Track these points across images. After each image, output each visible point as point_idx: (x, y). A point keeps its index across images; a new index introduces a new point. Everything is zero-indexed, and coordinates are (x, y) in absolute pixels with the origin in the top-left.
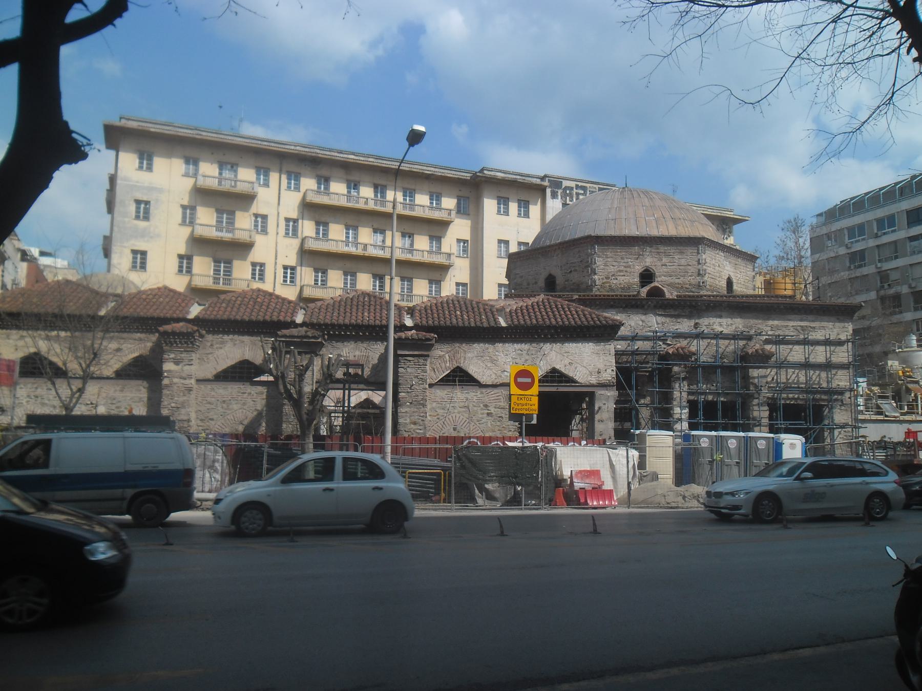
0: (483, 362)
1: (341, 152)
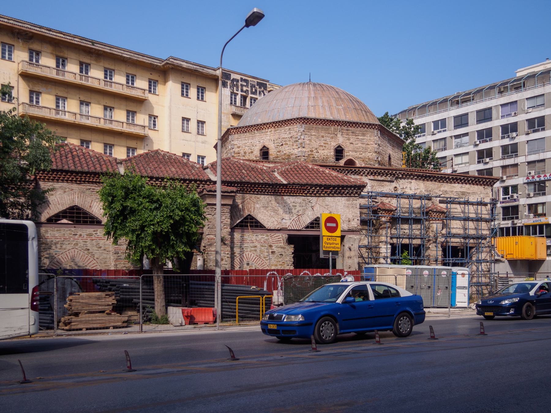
0: (267, 211)
1: (50, 30)
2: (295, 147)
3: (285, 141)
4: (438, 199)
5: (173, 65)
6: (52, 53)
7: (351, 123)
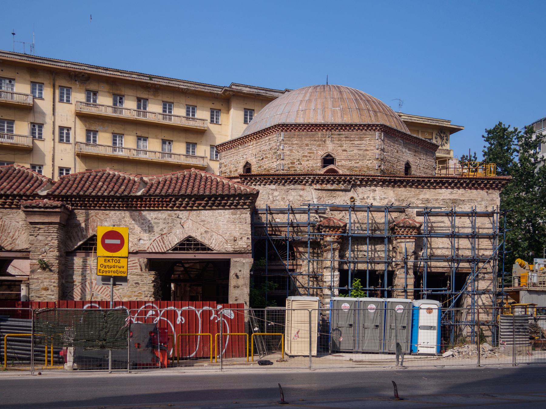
3: (265, 154)
4: (416, 210)
5: (234, 91)
6: (109, 92)
7: (343, 125)
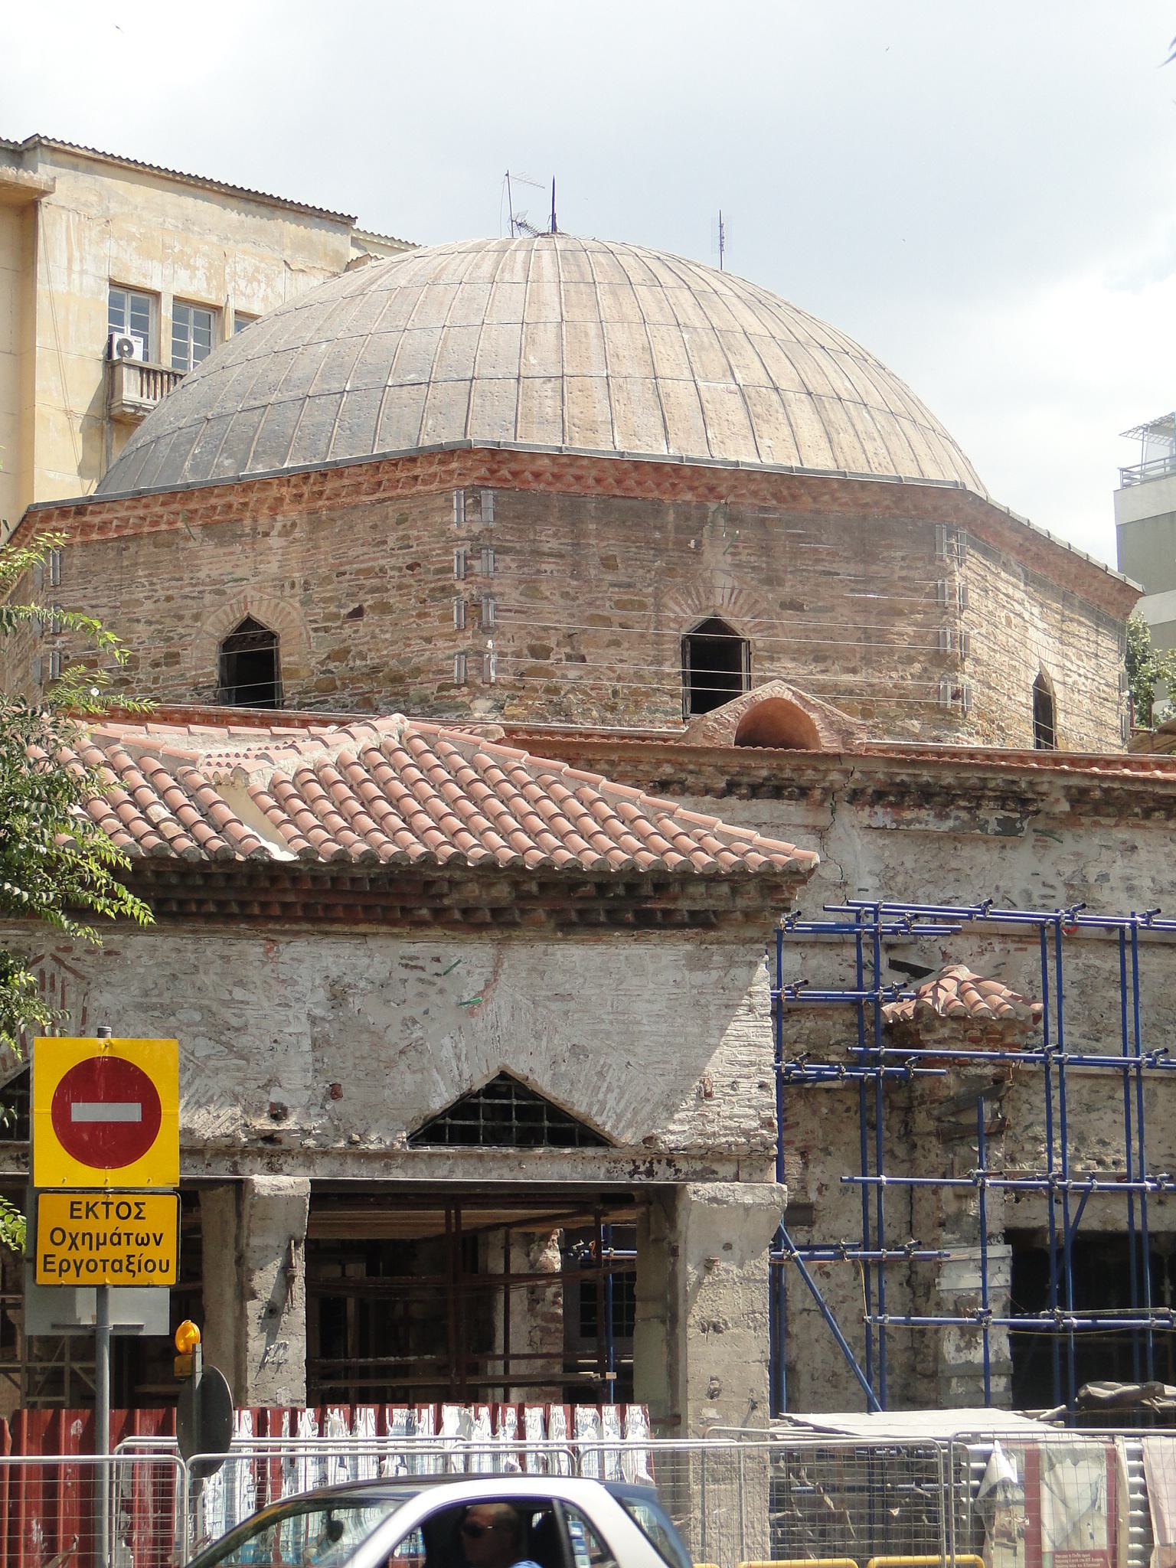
2: (433, 624)
